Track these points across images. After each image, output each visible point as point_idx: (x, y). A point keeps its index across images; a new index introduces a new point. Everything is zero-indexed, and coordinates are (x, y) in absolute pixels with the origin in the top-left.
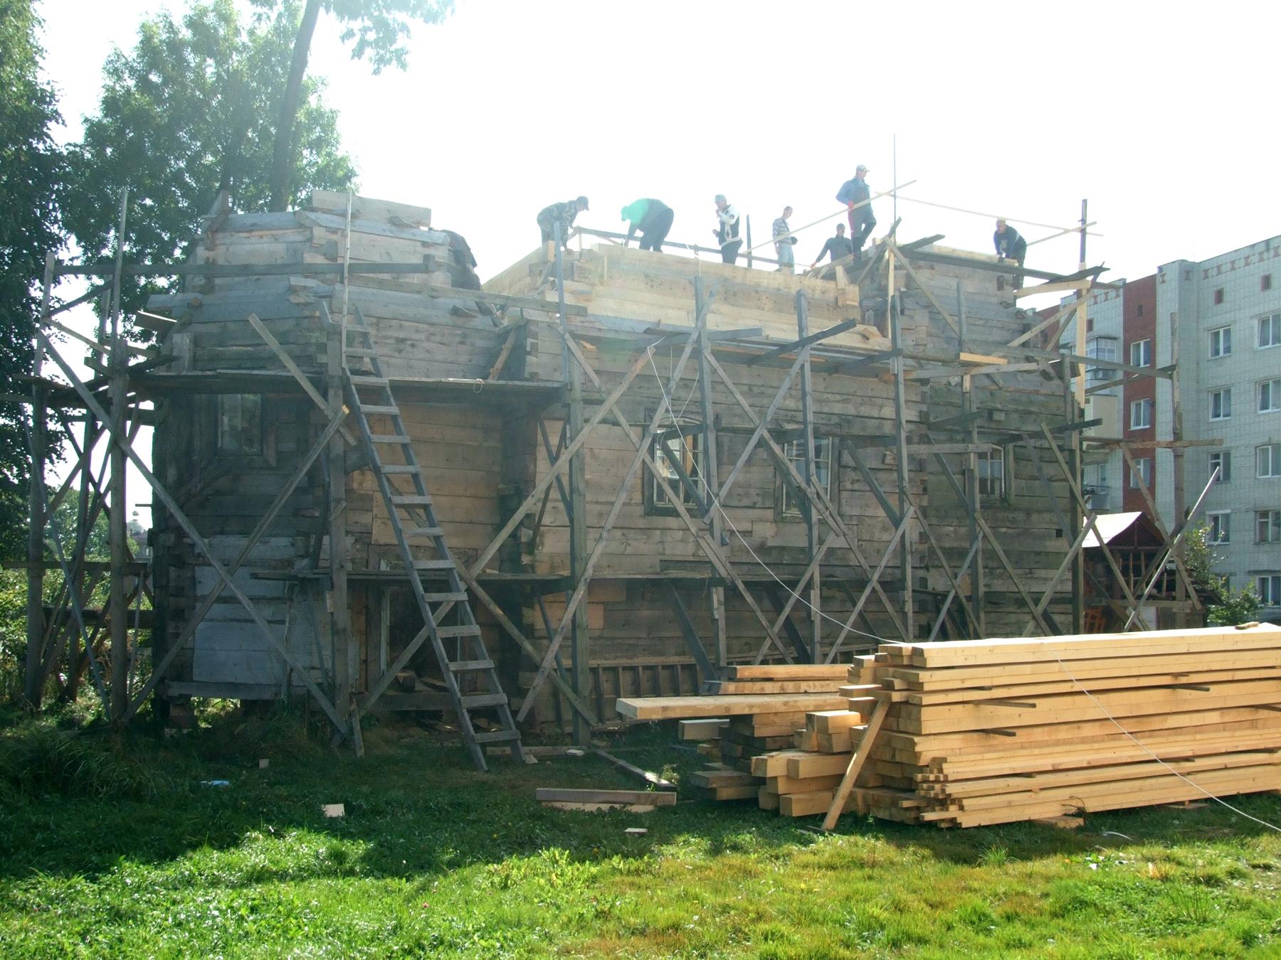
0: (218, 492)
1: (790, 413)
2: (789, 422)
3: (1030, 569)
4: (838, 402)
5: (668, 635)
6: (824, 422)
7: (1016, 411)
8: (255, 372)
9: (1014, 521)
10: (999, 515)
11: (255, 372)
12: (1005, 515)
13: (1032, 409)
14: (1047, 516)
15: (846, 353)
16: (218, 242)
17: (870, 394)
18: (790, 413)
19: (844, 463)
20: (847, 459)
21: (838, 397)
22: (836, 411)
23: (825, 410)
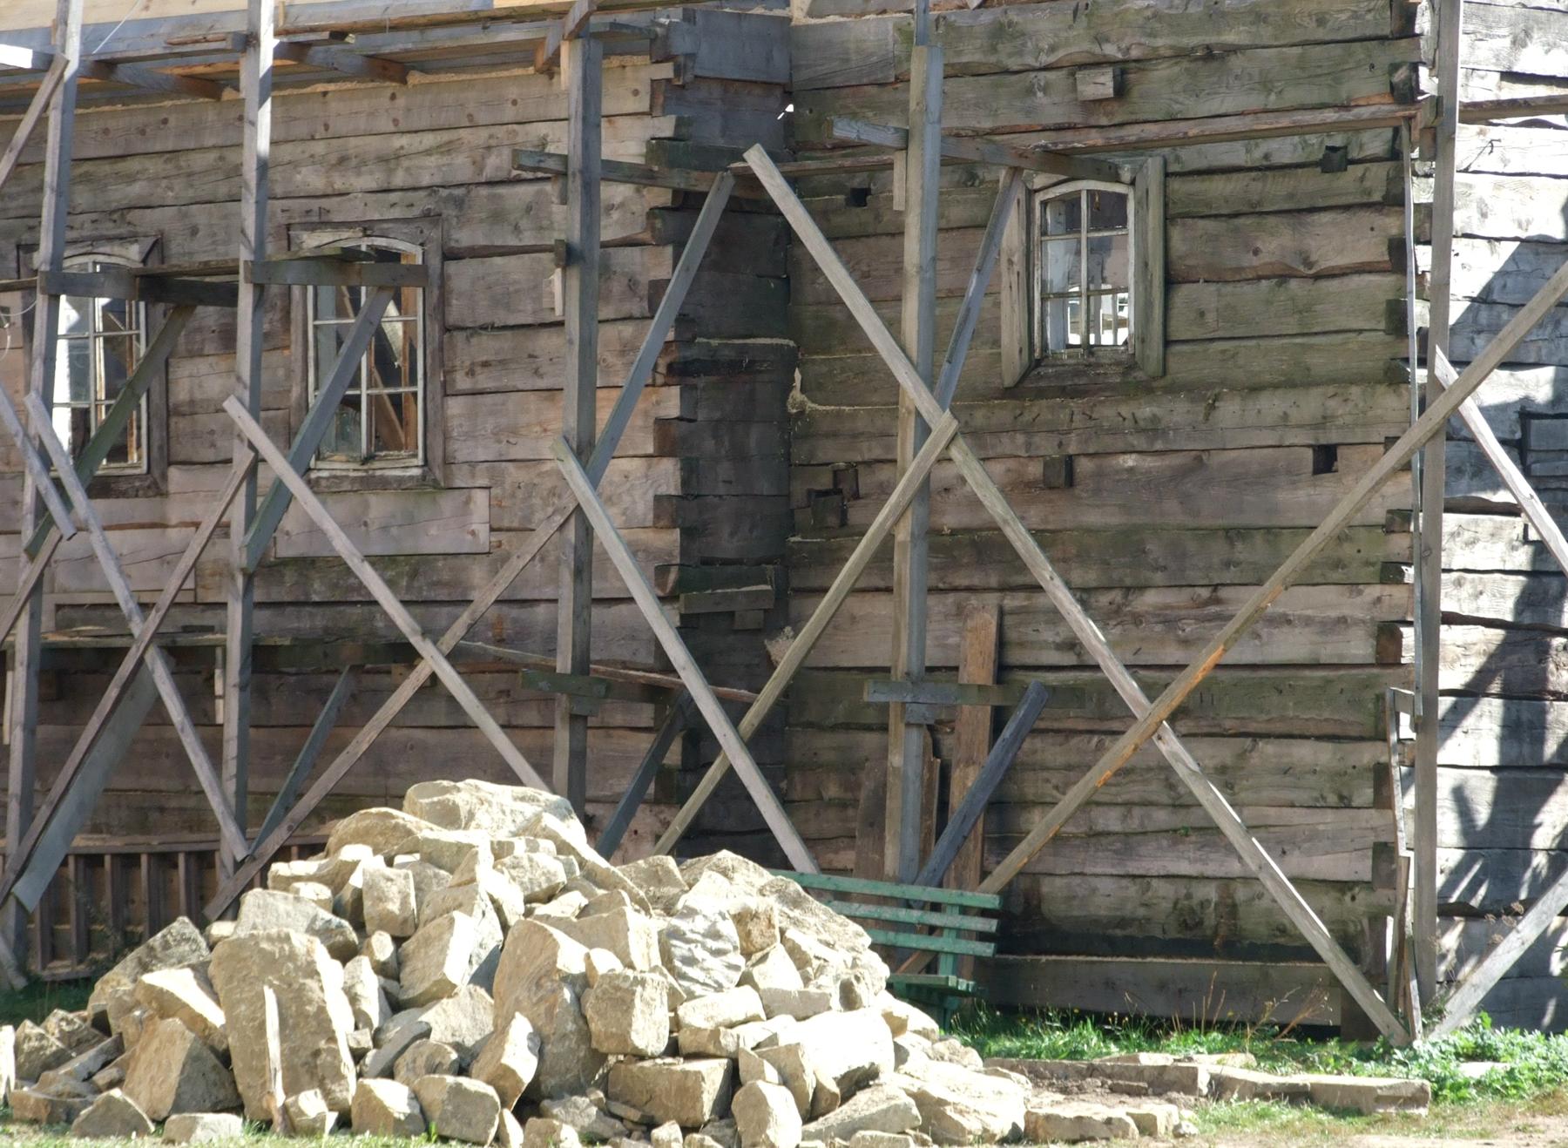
0: (1096, 836)
1: (315, 204)
2: (313, 227)
3: (1216, 587)
4: (428, 152)
5: (1099, 870)
6: (396, 213)
7: (1180, 54)
8: (208, 279)
9: (1153, 429)
10: (1108, 413)
11: (208, 279)
12: (1125, 410)
13: (1230, 38)
14: (1272, 405)
15: (396, 27)
16: (592, 43)
17: (509, 113)
18: (315, 204)
19: (453, 317)
20: (1092, 287)
21: (429, 140)
22: (426, 180)
23: (399, 179)
